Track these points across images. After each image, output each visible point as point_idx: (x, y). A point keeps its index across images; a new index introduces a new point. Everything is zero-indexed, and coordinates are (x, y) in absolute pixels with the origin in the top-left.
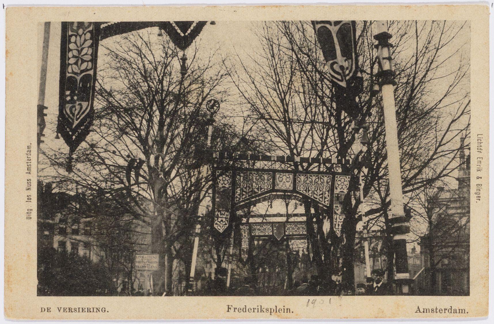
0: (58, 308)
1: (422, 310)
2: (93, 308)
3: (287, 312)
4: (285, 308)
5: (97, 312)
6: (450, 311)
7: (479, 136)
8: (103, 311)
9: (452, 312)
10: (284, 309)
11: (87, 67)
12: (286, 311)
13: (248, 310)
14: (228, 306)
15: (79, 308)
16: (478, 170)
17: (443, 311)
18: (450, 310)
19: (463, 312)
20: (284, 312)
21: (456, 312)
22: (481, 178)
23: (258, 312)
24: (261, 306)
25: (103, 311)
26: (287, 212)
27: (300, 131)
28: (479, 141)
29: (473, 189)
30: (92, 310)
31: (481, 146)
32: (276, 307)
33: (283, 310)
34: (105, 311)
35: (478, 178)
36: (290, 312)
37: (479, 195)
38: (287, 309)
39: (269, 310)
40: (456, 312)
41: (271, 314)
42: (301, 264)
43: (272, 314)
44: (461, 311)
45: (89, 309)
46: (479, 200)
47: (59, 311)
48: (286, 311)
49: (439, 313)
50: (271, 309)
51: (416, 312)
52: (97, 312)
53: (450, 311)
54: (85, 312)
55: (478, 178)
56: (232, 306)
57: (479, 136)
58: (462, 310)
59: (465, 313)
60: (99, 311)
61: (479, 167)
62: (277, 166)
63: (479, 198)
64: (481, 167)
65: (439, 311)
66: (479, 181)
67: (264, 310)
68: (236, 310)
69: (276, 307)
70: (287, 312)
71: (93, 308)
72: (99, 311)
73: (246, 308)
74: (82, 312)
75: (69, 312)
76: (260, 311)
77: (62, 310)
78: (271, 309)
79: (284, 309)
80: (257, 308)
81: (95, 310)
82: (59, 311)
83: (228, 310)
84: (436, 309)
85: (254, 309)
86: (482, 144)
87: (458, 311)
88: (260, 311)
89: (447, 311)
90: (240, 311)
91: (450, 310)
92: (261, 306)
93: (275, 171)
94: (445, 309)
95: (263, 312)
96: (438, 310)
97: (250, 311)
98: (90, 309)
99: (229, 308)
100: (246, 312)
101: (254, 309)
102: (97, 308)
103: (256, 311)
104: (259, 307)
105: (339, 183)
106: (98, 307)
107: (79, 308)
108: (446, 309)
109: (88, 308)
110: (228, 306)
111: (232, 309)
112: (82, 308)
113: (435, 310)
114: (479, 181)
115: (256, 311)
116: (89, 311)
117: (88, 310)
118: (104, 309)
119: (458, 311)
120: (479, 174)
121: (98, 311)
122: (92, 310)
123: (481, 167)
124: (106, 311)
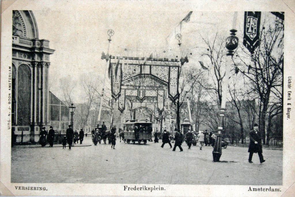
0: (16, 187)
1: (252, 189)
2: (38, 188)
3: (161, 190)
6: (135, 189)
7: (289, 78)
8: (44, 190)
10: (160, 188)
11: (44, 48)
13: (137, 189)
14: (16, 187)
15: (29, 187)
16: (288, 99)
17: (140, 189)
18: (270, 190)
19: (278, 190)
21: (273, 191)
22: (290, 104)
24: (145, 186)
26: (22, 141)
27: (114, 88)
29: (285, 111)
30: (37, 189)
32: (155, 186)
34: (45, 189)
35: (288, 104)
36: (163, 190)
37: (289, 115)
38: (162, 188)
39: (150, 188)
40: (273, 191)
43: (152, 191)
44: (276, 190)
45: (35, 188)
46: (289, 118)
47: (16, 189)
51: (249, 191)
53: (135, 189)
54: (32, 190)
55: (288, 104)
56: (127, 186)
57: (289, 78)
58: (255, 189)
60: (41, 190)
61: (289, 97)
62: (171, 64)
66: (289, 106)
67: (147, 189)
69: (155, 186)
73: (135, 188)
75: (23, 189)
76: (144, 189)
77: (18, 188)
79: (160, 188)
80: (142, 187)
82: (16, 189)
83: (125, 189)
85: (141, 188)
87: (274, 190)
89: (268, 190)
90: (132, 189)
91: (270, 190)
92: (145, 186)
94: (266, 189)
95: (147, 190)
96: (262, 189)
98: (36, 188)
99: (125, 188)
100: (136, 190)
101: (141, 188)
102: (40, 188)
104: (144, 187)
107: (29, 187)
109: (34, 188)
110: (125, 186)
111: (127, 189)
112: (31, 187)
113: (260, 189)
114: (289, 106)
116: (35, 189)
117: (34, 189)
118: (44, 188)
119: (274, 190)
120: (289, 102)
121: (40, 189)
124: (46, 190)
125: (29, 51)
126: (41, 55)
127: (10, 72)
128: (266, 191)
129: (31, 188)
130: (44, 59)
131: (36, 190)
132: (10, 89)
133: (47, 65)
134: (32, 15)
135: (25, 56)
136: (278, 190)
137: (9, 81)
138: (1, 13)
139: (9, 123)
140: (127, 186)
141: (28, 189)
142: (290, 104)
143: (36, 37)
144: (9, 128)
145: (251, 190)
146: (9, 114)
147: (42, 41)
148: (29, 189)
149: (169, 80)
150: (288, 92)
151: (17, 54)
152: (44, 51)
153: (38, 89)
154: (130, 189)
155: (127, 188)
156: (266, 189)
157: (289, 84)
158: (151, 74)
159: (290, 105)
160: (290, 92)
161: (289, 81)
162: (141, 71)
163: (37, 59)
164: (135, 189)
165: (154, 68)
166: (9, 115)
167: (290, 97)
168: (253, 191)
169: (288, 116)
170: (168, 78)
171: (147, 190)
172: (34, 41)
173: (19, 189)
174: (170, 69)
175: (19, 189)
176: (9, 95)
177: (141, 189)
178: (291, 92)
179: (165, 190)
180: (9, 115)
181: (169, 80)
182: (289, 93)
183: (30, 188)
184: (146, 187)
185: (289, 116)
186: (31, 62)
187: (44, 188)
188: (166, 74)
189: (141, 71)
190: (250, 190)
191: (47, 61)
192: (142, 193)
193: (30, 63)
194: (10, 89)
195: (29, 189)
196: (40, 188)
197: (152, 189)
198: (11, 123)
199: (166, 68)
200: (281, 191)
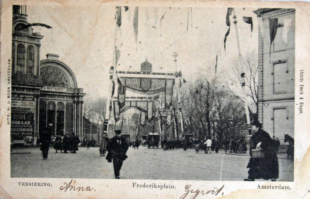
0: (19, 183)
1: (261, 187)
2: (42, 183)
3: (172, 188)
4: (171, 185)
5: (44, 186)
6: (279, 188)
8: (49, 185)
9: (281, 188)
12: (171, 187)
15: (33, 183)
19: (288, 188)
20: (170, 188)
21: (283, 189)
22: (303, 98)
23: (153, 187)
24: (155, 184)
25: (49, 185)
28: (302, 75)
30: (41, 184)
31: (303, 78)
32: (165, 184)
33: (169, 187)
34: (50, 185)
35: (301, 98)
38: (172, 186)
39: (160, 186)
40: (283, 189)
41: (137, 187)
42: (119, 142)
45: (27, 183)
46: (302, 113)
48: (171, 187)
49: (272, 188)
50: (161, 186)
52: (44, 186)
53: (279, 188)
55: (301, 98)
56: (136, 183)
59: (289, 189)
60: (46, 185)
61: (301, 91)
62: (148, 100)
63: (301, 112)
64: (303, 91)
65: (272, 187)
66: (302, 101)
67: (157, 186)
68: (139, 186)
69: (165, 184)
70: (172, 188)
71: (42, 183)
72: (46, 185)
73: (145, 185)
74: (35, 185)
75: (26, 185)
76: (154, 187)
77: (21, 184)
78: (161, 186)
81: (43, 185)
82: (20, 185)
84: (270, 186)
86: (303, 77)
88: (154, 187)
89: (277, 188)
90: (141, 187)
92: (155, 184)
93: (148, 101)
94: (276, 187)
95: (156, 187)
96: (271, 187)
97: (147, 187)
99: (133, 185)
100: (145, 187)
102: (44, 184)
103: (151, 187)
104: (154, 184)
105: (168, 83)
106: (45, 183)
107: (33, 183)
108: (277, 187)
109: (38, 183)
110: (133, 183)
113: (269, 187)
114: (302, 101)
115: (151, 187)
116: (39, 185)
117: (38, 184)
118: (49, 184)
119: (284, 188)
120: (302, 96)
122: (41, 184)
123: (303, 91)
124: (50, 185)
125: (71, 95)
126: (78, 97)
127: (9, 65)
128: (276, 189)
129: (39, 184)
130: (80, 100)
131: (40, 185)
132: (9, 83)
133: (82, 102)
134: (63, 64)
135: (70, 98)
136: (288, 188)
137: (8, 75)
138: (1, 16)
139: (8, 118)
140: (136, 183)
141: (32, 185)
142: (303, 98)
143: (76, 87)
144: (8, 123)
145: (260, 188)
146: (9, 108)
147: (79, 89)
148: (33, 185)
149: (147, 110)
150: (300, 85)
151: (65, 97)
152: (79, 95)
153: (79, 116)
154: (138, 186)
155: (135, 184)
156: (276, 187)
157: (302, 77)
158: (136, 106)
159: (302, 99)
160: (302, 86)
161: (302, 75)
162: (131, 104)
163: (76, 99)
164: (144, 186)
165: (138, 103)
166: (8, 110)
167: (302, 91)
168: (262, 188)
169: (300, 111)
170: (146, 108)
171: (156, 187)
172: (75, 89)
173: (23, 185)
174: (148, 102)
175: (23, 185)
176: (8, 89)
177: (151, 187)
178: (303, 85)
179: (175, 188)
180: (8, 110)
181: (147, 110)
182: (301, 86)
183: (34, 184)
184: (156, 184)
185: (302, 111)
186: (73, 101)
187: (49, 184)
188: (145, 105)
189: (131, 104)
190: (259, 188)
191: (81, 100)
192: (151, 190)
193: (72, 102)
194: (9, 83)
195: (33, 185)
196: (44, 184)
197: (162, 187)
198: (10, 118)
199: (146, 103)
200: (291, 189)
